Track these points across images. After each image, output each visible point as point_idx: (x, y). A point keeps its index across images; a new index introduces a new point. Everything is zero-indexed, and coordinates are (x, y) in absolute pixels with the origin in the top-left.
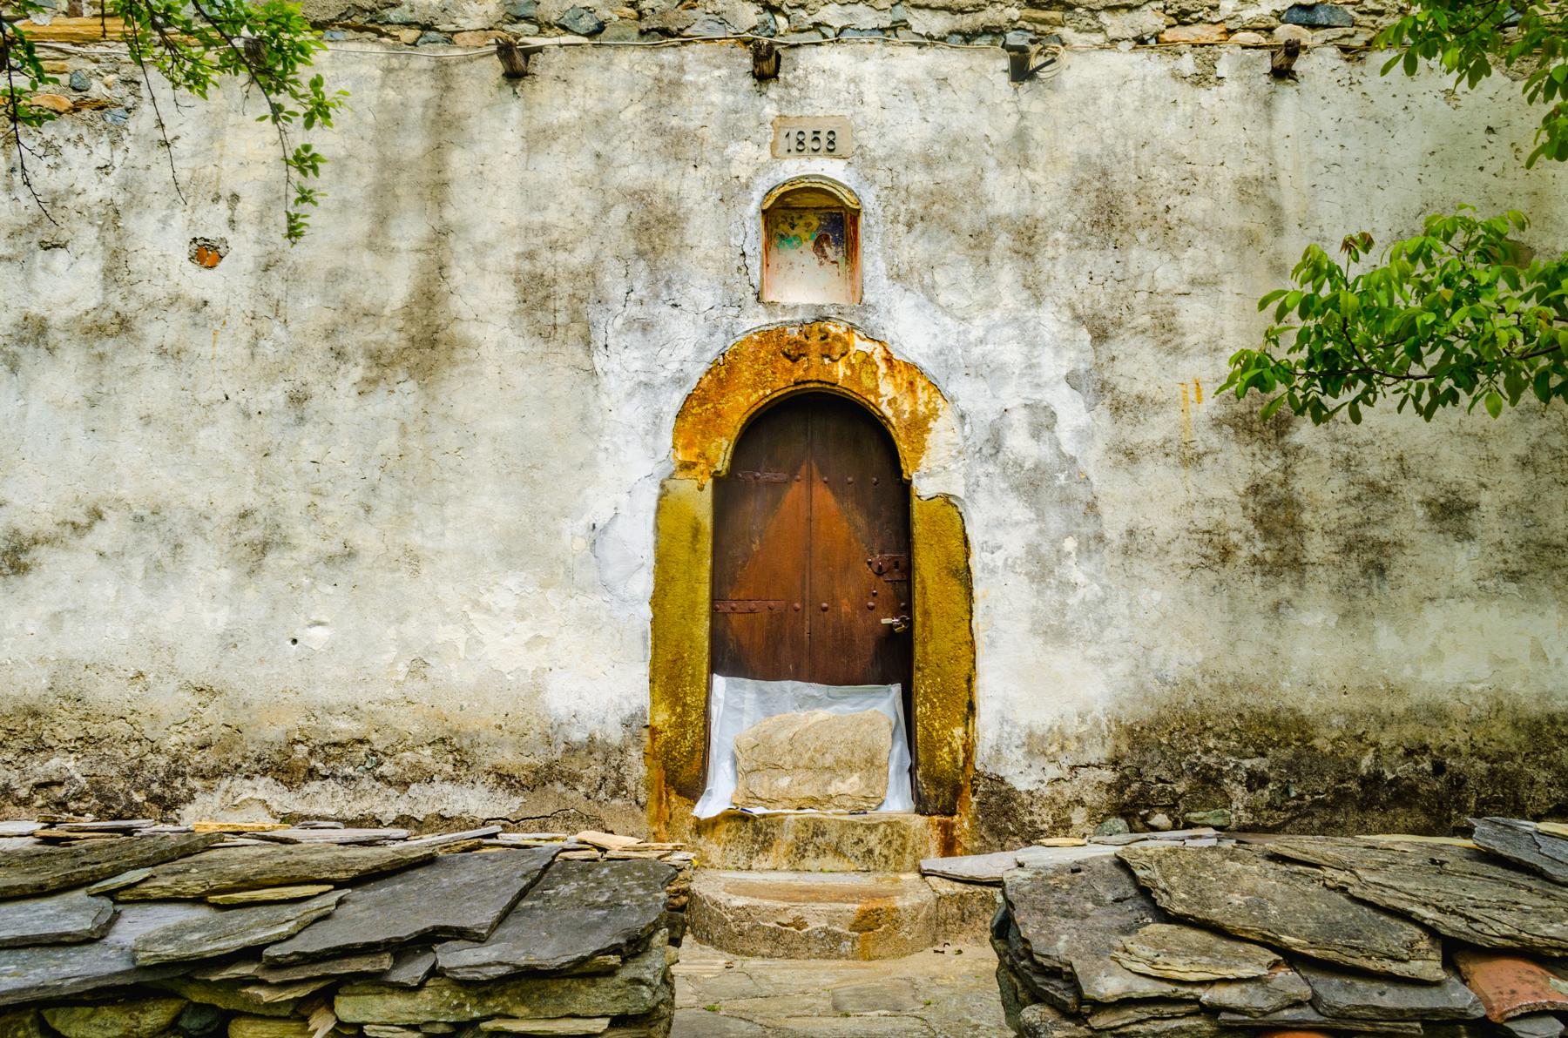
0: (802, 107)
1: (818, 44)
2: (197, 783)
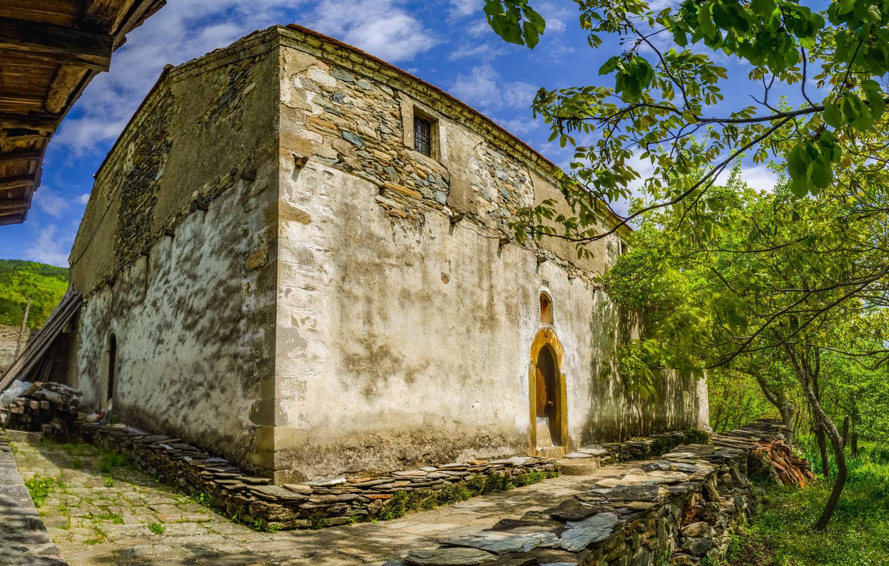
2: (458, 451)
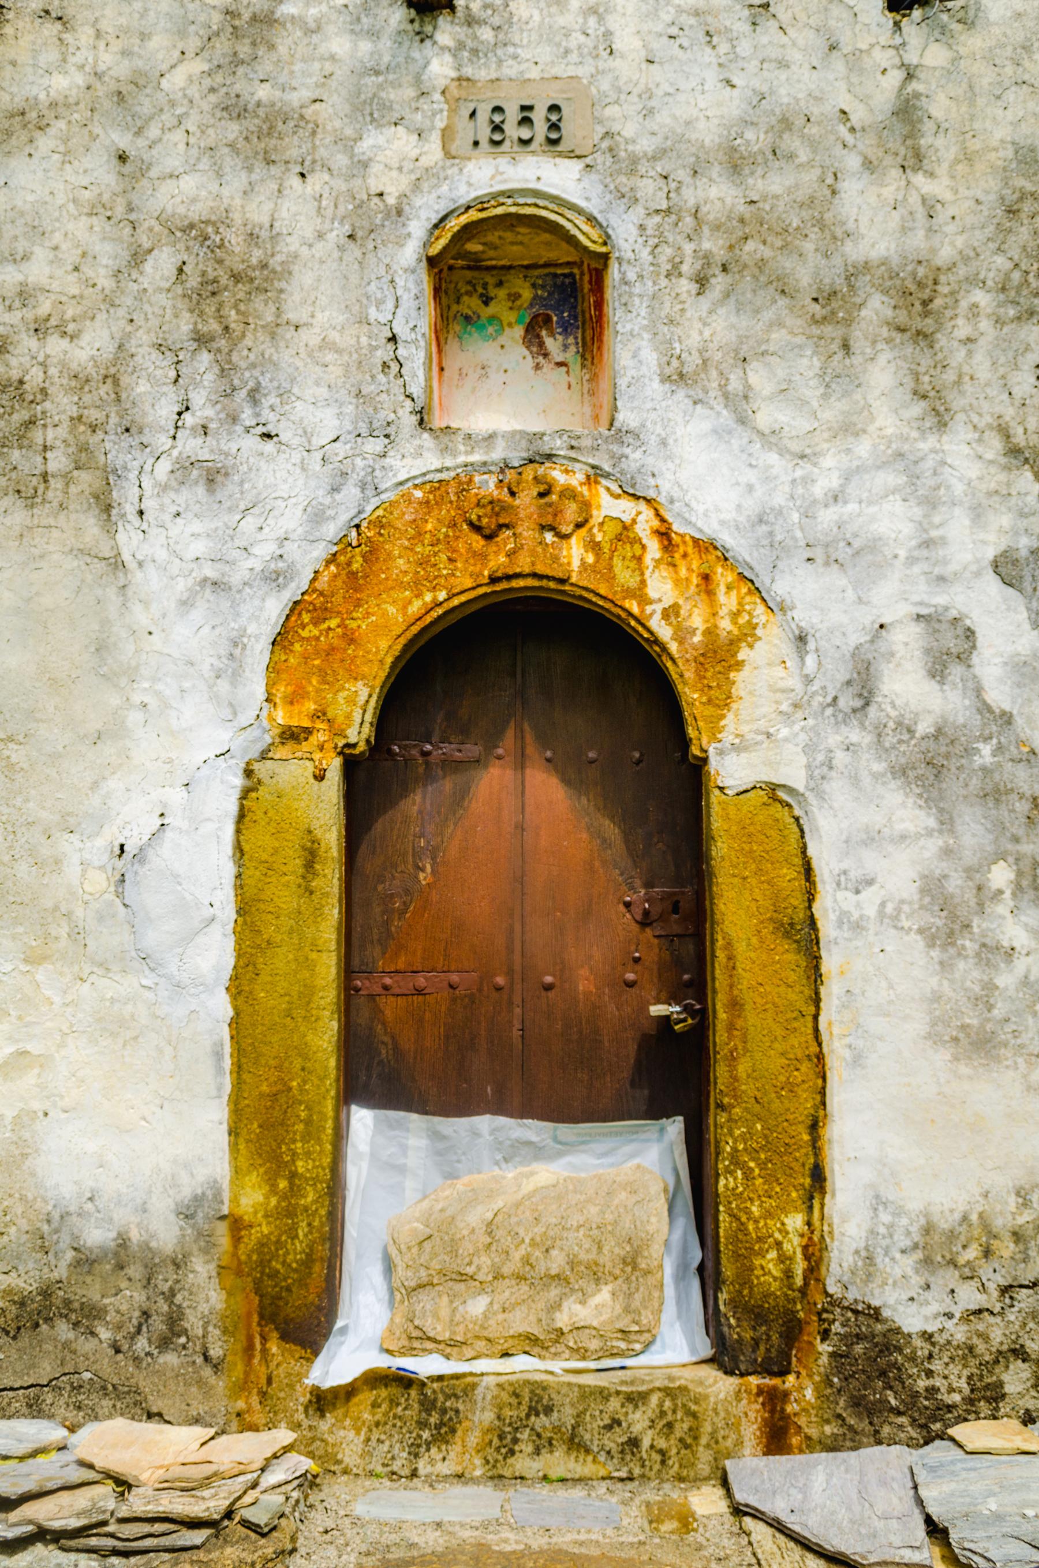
0: (500, 62)
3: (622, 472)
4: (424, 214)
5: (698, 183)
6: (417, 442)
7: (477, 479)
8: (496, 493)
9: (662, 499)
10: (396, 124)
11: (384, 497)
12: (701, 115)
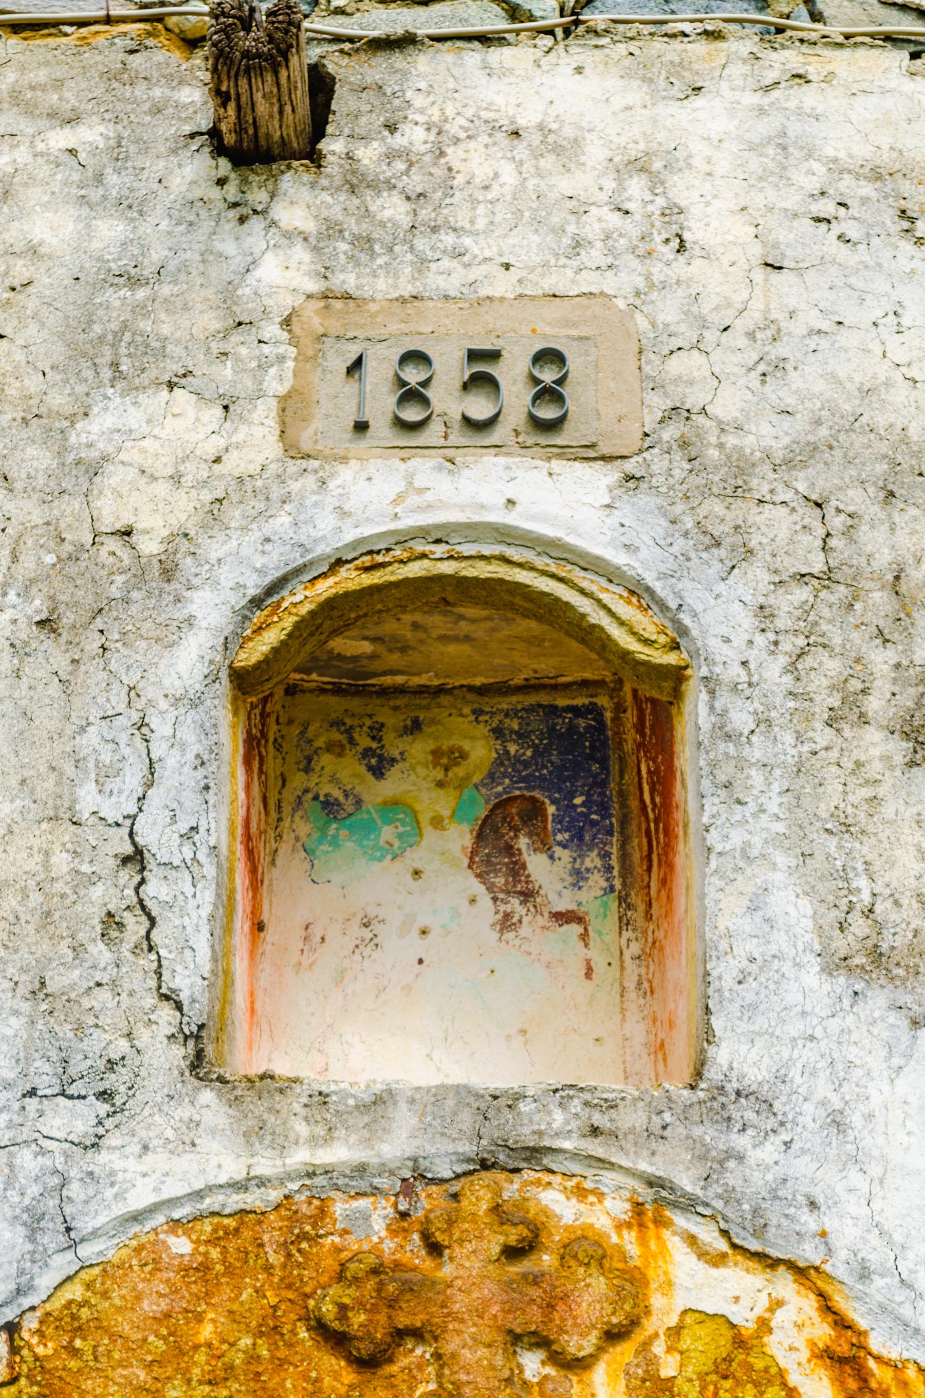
0: (422, 263)
1: (484, 39)
3: (728, 1197)
4: (227, 576)
5: (897, 518)
6: (185, 1112)
7: (340, 1208)
8: (389, 1246)
9: (837, 1268)
10: (171, 386)
11: (87, 1251)
12: (897, 376)
